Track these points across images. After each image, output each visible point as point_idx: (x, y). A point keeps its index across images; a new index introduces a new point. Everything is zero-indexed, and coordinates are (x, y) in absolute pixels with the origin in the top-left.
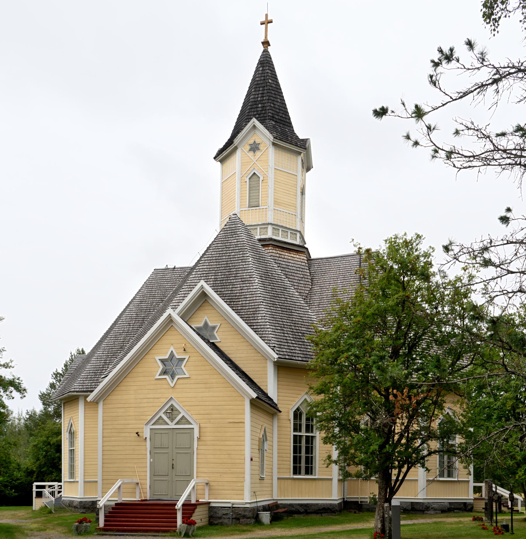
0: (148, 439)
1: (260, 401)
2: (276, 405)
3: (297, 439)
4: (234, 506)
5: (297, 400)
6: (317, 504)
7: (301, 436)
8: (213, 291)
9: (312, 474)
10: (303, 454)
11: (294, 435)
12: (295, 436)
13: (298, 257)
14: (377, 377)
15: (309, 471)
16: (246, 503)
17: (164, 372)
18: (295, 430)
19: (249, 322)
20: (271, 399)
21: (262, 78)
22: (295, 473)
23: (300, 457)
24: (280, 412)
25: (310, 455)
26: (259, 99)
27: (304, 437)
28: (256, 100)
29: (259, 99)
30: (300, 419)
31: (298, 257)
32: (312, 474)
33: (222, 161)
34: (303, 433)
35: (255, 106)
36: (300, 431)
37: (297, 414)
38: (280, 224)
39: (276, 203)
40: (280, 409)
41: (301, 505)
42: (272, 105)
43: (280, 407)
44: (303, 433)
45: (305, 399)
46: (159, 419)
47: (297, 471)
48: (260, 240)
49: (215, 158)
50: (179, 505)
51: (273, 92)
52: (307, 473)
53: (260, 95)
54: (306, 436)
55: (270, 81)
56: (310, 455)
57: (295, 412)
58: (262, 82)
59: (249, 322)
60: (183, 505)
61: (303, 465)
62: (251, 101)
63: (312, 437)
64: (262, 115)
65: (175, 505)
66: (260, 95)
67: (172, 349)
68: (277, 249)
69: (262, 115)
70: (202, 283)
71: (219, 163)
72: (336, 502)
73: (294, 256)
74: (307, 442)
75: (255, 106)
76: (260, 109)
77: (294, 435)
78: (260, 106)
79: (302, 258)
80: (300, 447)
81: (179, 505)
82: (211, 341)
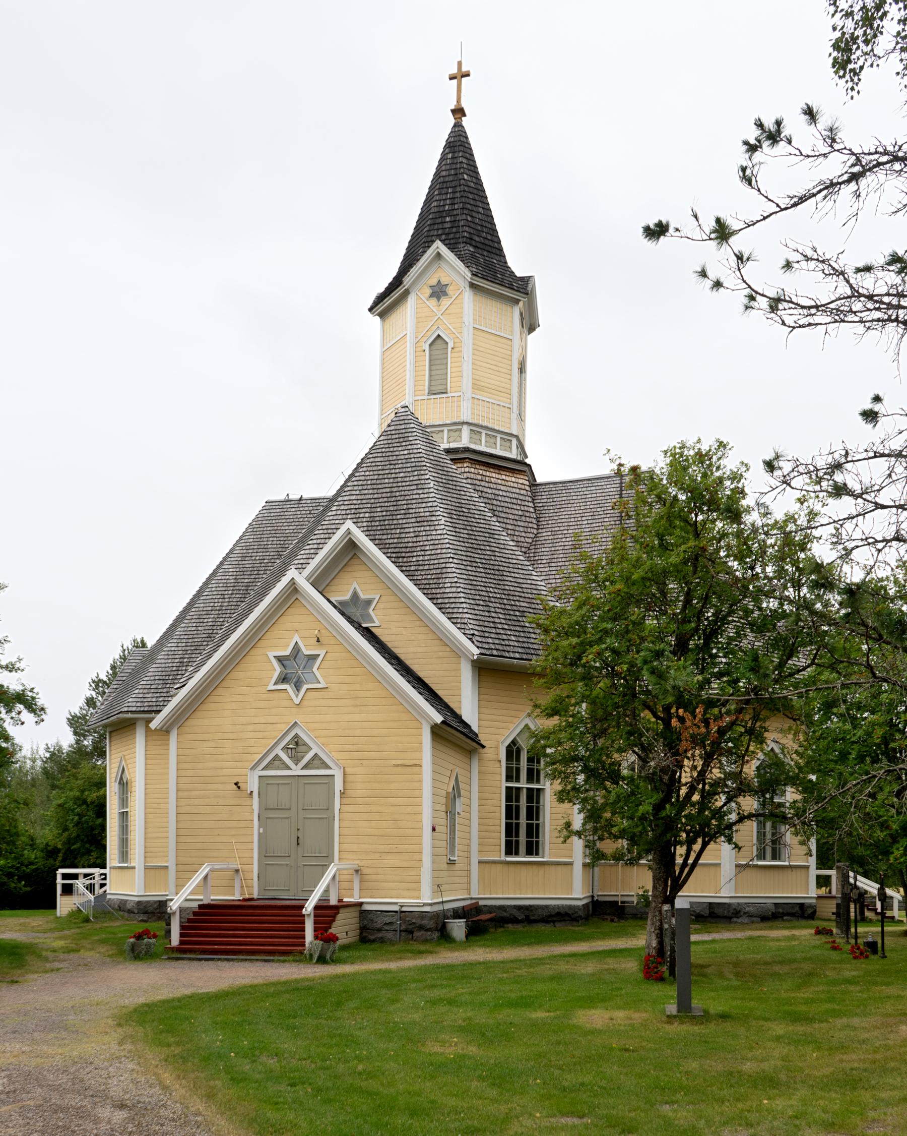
2: (477, 735)
3: (512, 795)
4: (404, 909)
6: (547, 906)
7: (518, 789)
8: (366, 539)
9: (537, 854)
10: (523, 820)
11: (507, 787)
12: (508, 789)
13: (513, 479)
15: (533, 848)
16: (425, 904)
17: (283, 679)
18: (509, 778)
19: (429, 591)
21: (453, 172)
22: (509, 852)
24: (483, 747)
25: (535, 822)
26: (447, 208)
27: (525, 790)
28: (442, 209)
29: (447, 208)
30: (518, 759)
31: (513, 479)
32: (537, 854)
33: (382, 315)
34: (523, 784)
35: (440, 220)
36: (518, 780)
37: (513, 752)
38: (484, 424)
39: (476, 386)
41: (520, 908)
42: (469, 218)
43: (482, 738)
44: (523, 784)
47: (511, 848)
48: (448, 451)
49: (370, 310)
50: (309, 907)
52: (529, 852)
53: (448, 202)
54: (528, 789)
55: (465, 177)
56: (535, 822)
57: (509, 747)
58: (451, 178)
60: (316, 908)
61: (523, 838)
62: (432, 211)
64: (452, 236)
65: (302, 907)
68: (478, 467)
71: (378, 318)
72: (580, 903)
73: (508, 478)
74: (530, 799)
75: (440, 220)
76: (448, 225)
77: (507, 787)
78: (448, 219)
79: (521, 481)
80: (518, 808)
81: (309, 907)
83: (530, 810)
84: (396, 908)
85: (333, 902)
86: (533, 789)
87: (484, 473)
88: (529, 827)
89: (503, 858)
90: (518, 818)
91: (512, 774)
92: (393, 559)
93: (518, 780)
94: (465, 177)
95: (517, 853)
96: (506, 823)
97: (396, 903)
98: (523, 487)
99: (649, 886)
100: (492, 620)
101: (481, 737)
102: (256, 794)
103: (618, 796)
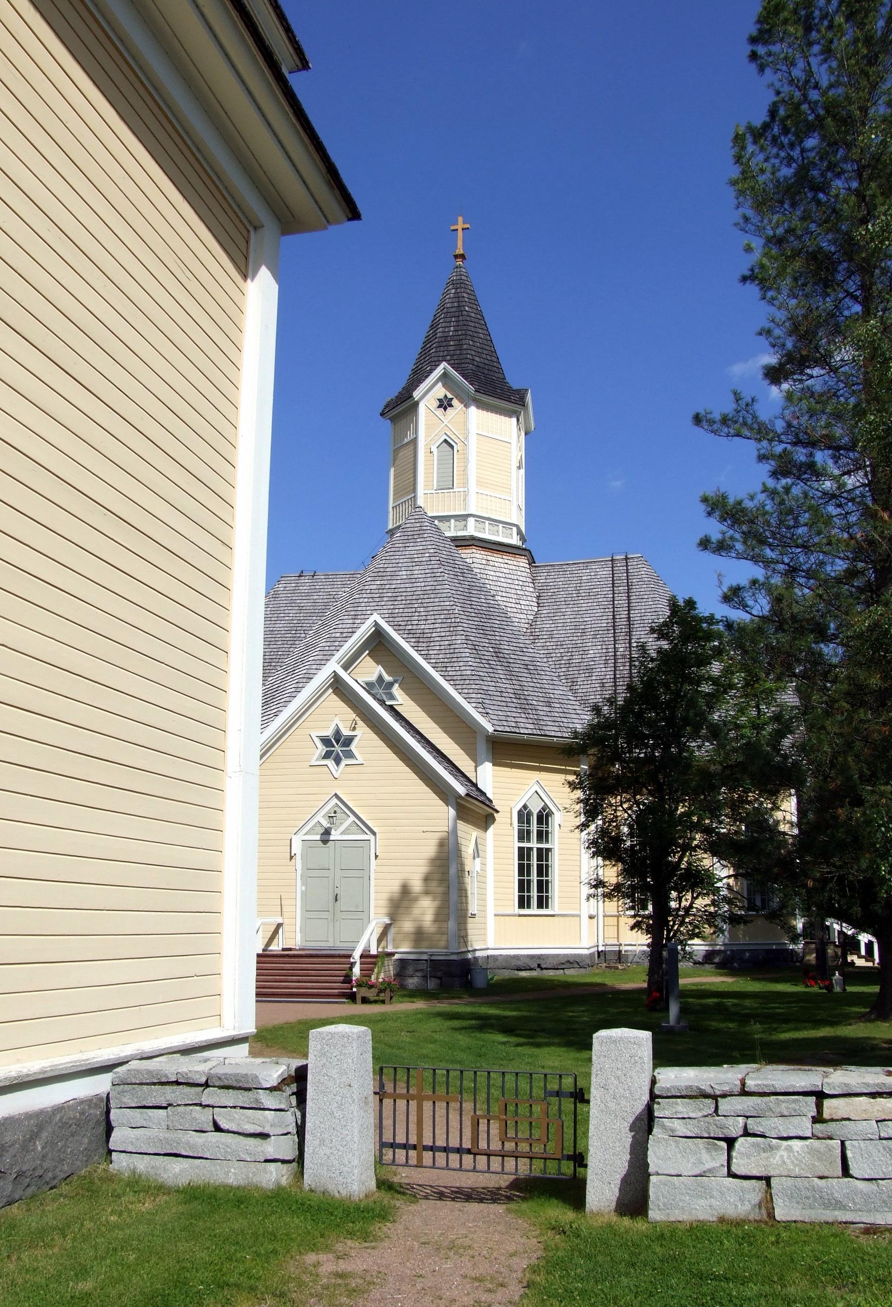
0: (298, 857)
1: (470, 799)
2: (491, 801)
3: (523, 854)
4: (433, 958)
5: (523, 793)
6: (557, 956)
7: (530, 849)
8: (411, 649)
9: (547, 907)
10: (534, 877)
11: (519, 848)
12: (521, 849)
13: (515, 563)
14: (804, 353)
15: (543, 902)
16: (452, 953)
17: (327, 756)
18: (521, 838)
19: (446, 674)
20: (484, 794)
21: (456, 304)
22: (521, 905)
23: (529, 881)
24: (497, 812)
25: (544, 878)
26: (451, 333)
27: (535, 850)
28: (446, 334)
29: (451, 333)
30: (528, 822)
31: (515, 563)
32: (547, 907)
33: (393, 420)
34: (534, 844)
35: (445, 344)
36: (529, 840)
37: (524, 815)
38: (487, 516)
39: (479, 483)
40: (496, 807)
41: (532, 957)
42: (471, 343)
43: (496, 804)
44: (534, 844)
45: (376, 624)
46: (315, 826)
47: (523, 902)
48: (454, 539)
49: (382, 414)
50: (357, 955)
51: (473, 324)
52: (540, 906)
53: (452, 329)
54: (538, 849)
55: (467, 308)
56: (544, 878)
57: (520, 813)
58: (454, 310)
59: (446, 674)
60: (362, 956)
61: (534, 893)
62: (438, 335)
63: (548, 850)
64: (455, 357)
65: (349, 956)
66: (452, 329)
67: (336, 721)
68: (482, 552)
69: (455, 357)
70: (376, 617)
71: (389, 421)
72: (586, 952)
73: (509, 562)
74: (540, 858)
75: (445, 344)
76: (452, 348)
77: (519, 848)
78: (452, 343)
79: (521, 564)
80: (529, 866)
81: (357, 955)
82: (388, 703)
83: (540, 867)
84: (425, 957)
85: (373, 952)
86: (542, 849)
87: (489, 558)
88: (540, 883)
89: (517, 911)
90: (529, 875)
91: (523, 835)
92: (412, 644)
93: (529, 840)
94: (467, 308)
95: (529, 907)
96: (519, 880)
97: (426, 953)
98: (523, 569)
99: (560, 778)
100: (503, 699)
101: (494, 803)
102: (298, 857)
103: (812, 619)
